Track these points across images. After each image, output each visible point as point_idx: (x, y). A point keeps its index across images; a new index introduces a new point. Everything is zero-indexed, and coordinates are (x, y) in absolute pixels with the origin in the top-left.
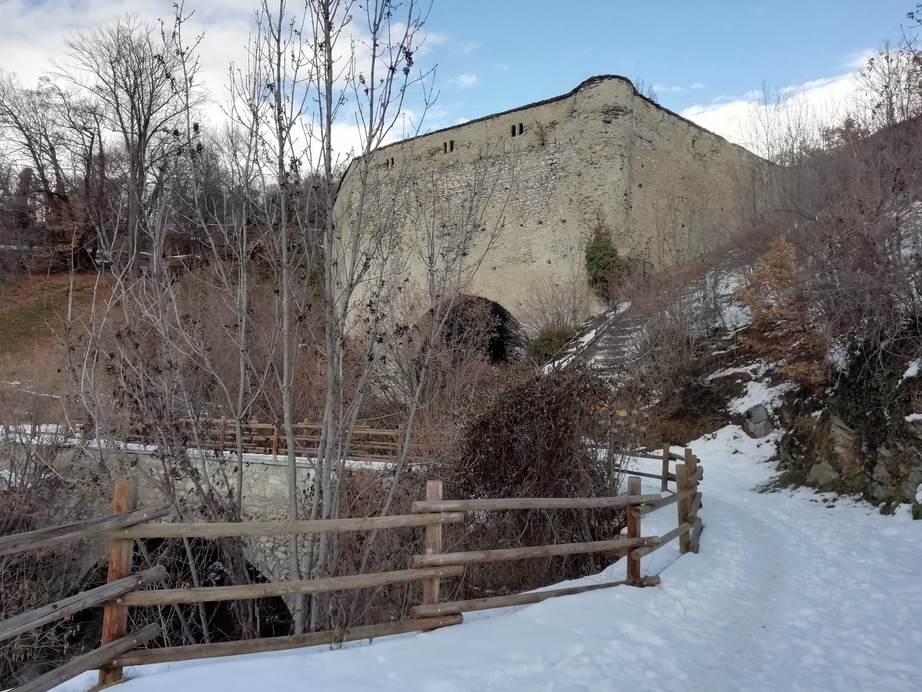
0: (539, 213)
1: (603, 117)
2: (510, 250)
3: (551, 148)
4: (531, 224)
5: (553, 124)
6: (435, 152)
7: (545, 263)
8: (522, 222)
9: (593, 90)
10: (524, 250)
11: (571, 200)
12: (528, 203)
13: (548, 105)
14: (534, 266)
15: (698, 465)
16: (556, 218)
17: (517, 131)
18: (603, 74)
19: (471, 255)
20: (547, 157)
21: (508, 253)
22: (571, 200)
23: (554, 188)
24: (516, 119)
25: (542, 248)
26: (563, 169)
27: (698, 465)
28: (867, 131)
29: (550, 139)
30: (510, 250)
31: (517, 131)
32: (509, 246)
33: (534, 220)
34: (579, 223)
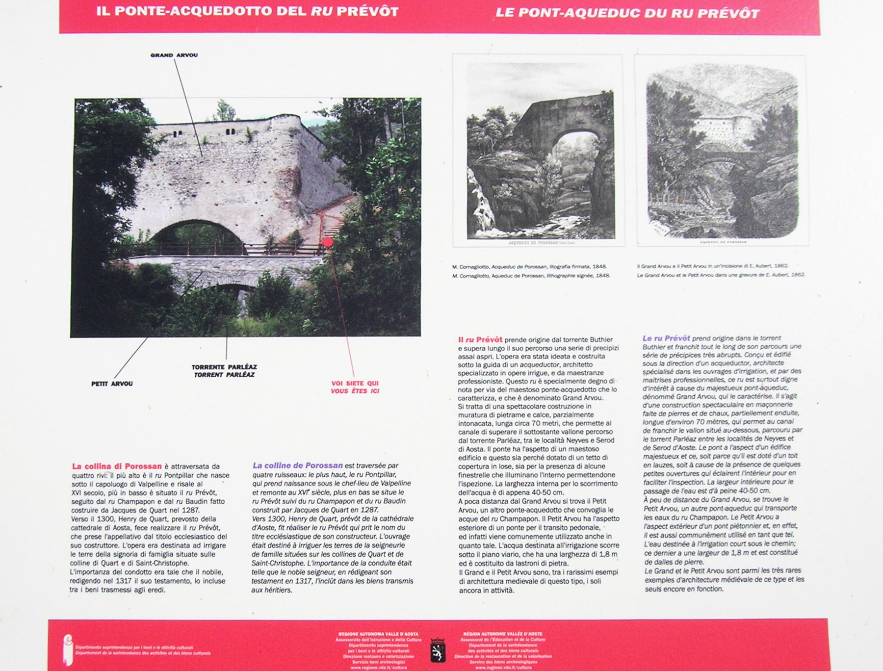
1: (289, 133)
3: (255, 144)
5: (256, 132)
8: (236, 181)
9: (284, 120)
11: (270, 172)
13: (252, 123)
17: (231, 132)
18: (289, 113)
20: (253, 148)
23: (258, 165)
29: (255, 138)
31: (231, 132)
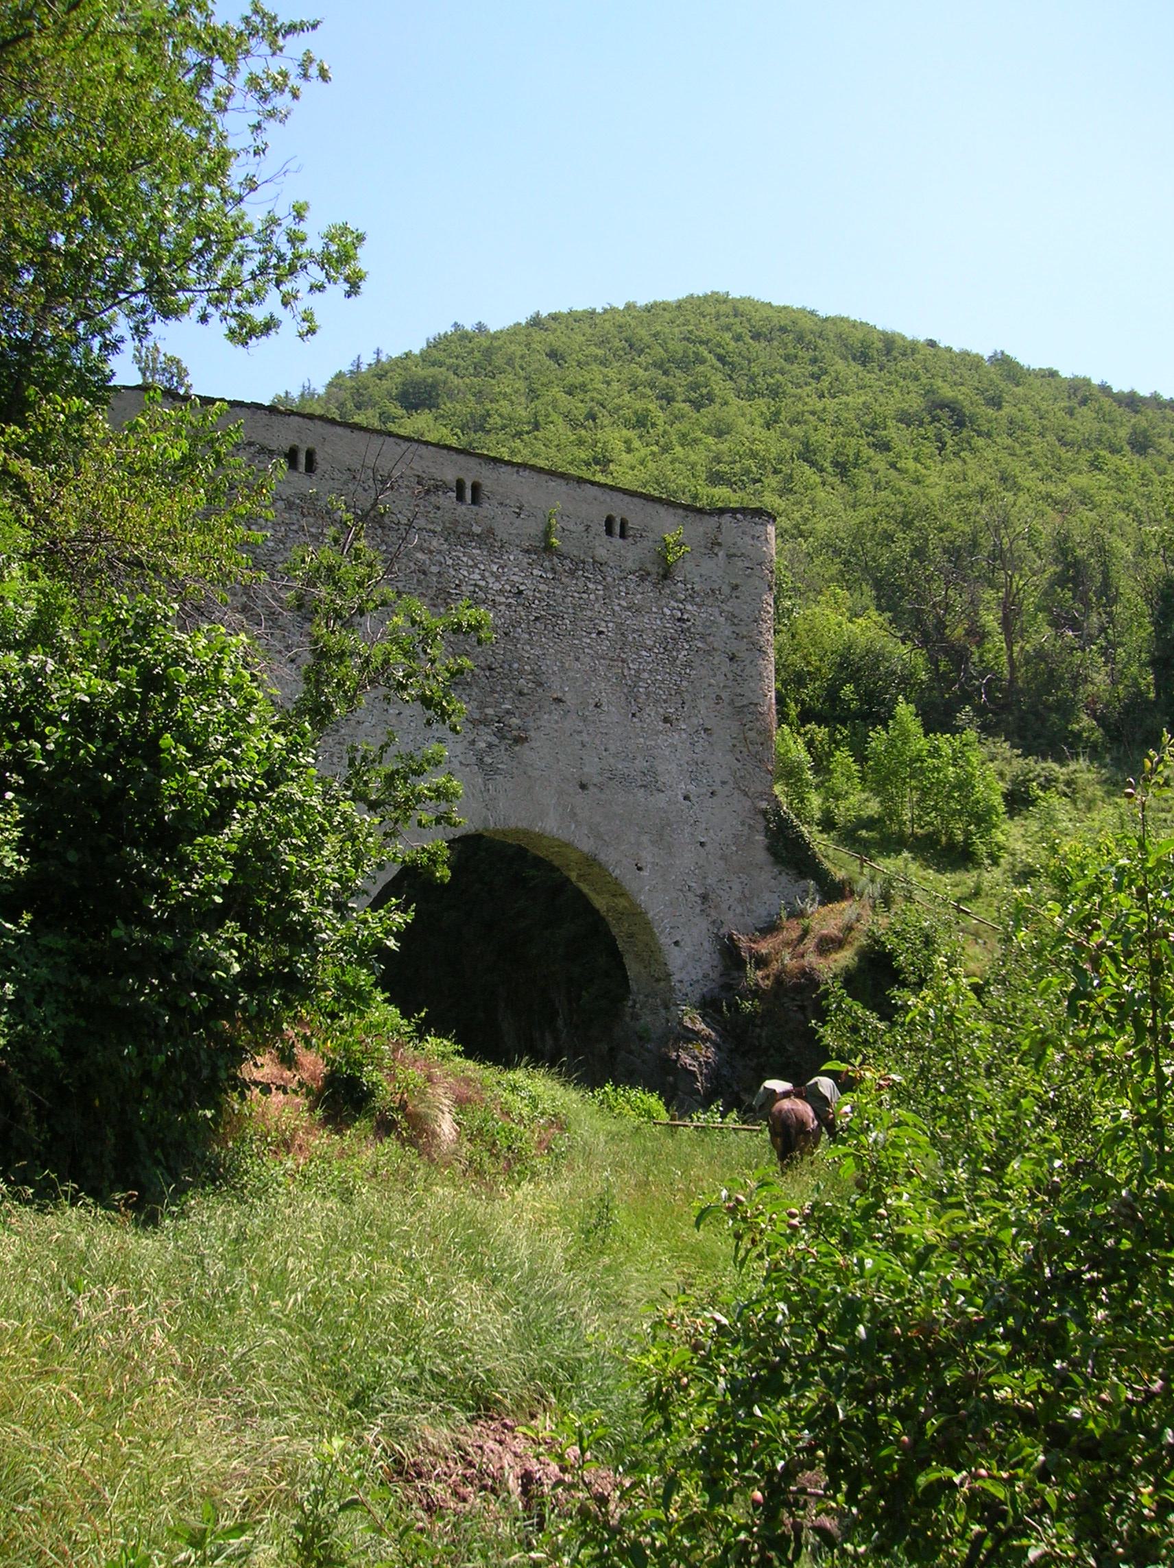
0: (665, 701)
2: (615, 755)
4: (652, 713)
6: (437, 488)
7: (681, 798)
10: (640, 764)
11: (719, 697)
12: (646, 675)
14: (661, 800)
15: (387, 994)
16: (695, 721)
19: (533, 744)
21: (612, 761)
22: (719, 697)
24: (621, 508)
25: (673, 767)
26: (703, 637)
27: (387, 994)
28: (616, 1085)
30: (615, 755)
32: (612, 749)
33: (657, 713)
34: (734, 741)
